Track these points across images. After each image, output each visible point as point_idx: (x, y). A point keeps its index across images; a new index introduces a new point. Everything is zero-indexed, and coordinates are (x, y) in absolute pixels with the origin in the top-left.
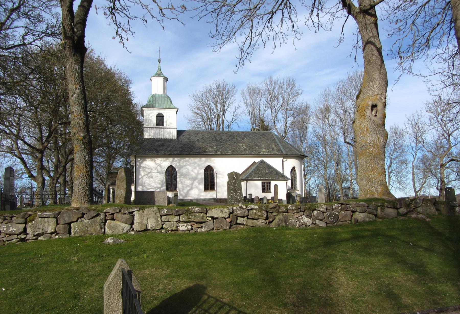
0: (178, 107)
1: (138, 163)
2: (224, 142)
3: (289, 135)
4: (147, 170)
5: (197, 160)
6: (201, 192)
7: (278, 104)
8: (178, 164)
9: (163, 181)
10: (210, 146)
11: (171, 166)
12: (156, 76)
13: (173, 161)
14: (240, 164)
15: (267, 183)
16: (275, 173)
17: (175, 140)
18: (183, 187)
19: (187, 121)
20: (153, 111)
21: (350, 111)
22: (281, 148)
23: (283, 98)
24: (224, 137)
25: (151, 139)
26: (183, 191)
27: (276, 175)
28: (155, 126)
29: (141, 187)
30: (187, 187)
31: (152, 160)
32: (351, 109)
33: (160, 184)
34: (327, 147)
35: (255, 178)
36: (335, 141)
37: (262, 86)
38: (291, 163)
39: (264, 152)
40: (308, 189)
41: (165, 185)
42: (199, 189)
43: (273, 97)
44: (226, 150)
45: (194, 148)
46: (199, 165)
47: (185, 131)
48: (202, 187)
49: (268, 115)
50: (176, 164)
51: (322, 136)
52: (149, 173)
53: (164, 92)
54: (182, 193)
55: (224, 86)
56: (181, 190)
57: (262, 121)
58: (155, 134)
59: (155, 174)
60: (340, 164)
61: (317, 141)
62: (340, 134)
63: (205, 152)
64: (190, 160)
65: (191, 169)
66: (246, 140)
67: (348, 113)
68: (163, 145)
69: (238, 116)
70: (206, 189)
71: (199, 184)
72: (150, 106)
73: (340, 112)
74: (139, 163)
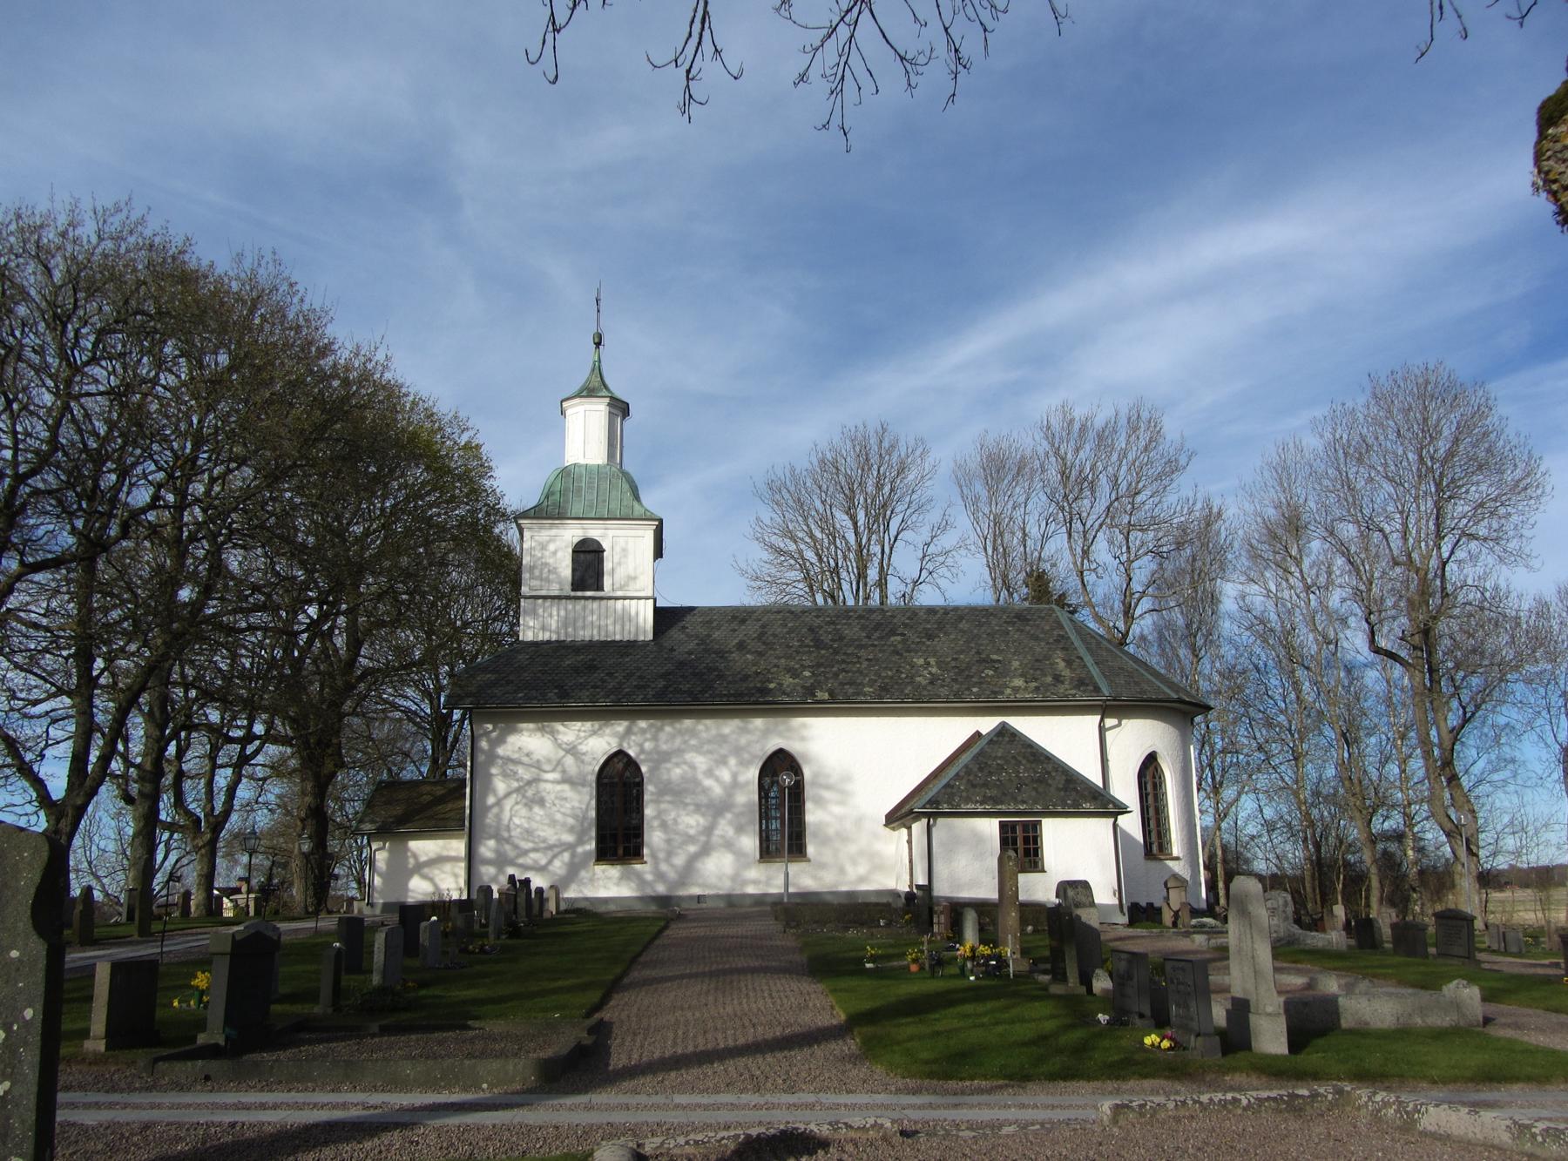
0: (660, 514)
1: (484, 744)
2: (855, 653)
3: (1144, 624)
4: (521, 771)
6: (747, 866)
7: (1094, 508)
10: (789, 670)
11: (620, 753)
12: (578, 395)
13: (628, 732)
15: (1025, 825)
16: (1060, 780)
17: (645, 644)
18: (668, 841)
19: (744, 581)
21: (1387, 529)
22: (1095, 671)
23: (1115, 484)
24: (852, 631)
25: (549, 642)
27: (1065, 789)
28: (568, 591)
29: (492, 843)
30: (685, 843)
31: (542, 730)
33: (571, 830)
34: (1300, 673)
35: (970, 807)
36: (1332, 647)
37: (1029, 442)
38: (1136, 738)
39: (1016, 690)
40: (1232, 840)
41: (593, 834)
42: (739, 854)
43: (1072, 488)
44: (851, 683)
45: (720, 677)
46: (737, 751)
48: (750, 843)
49: (1058, 553)
50: (641, 745)
51: (1278, 628)
52: (529, 783)
54: (664, 867)
55: (886, 444)
56: (661, 855)
57: (1039, 583)
58: (565, 623)
59: (551, 787)
60: (1357, 740)
62: (1352, 621)
63: (764, 691)
65: (704, 767)
66: (943, 644)
68: (591, 668)
69: (942, 565)
70: (767, 852)
71: (740, 829)
72: (549, 510)
73: (1349, 531)
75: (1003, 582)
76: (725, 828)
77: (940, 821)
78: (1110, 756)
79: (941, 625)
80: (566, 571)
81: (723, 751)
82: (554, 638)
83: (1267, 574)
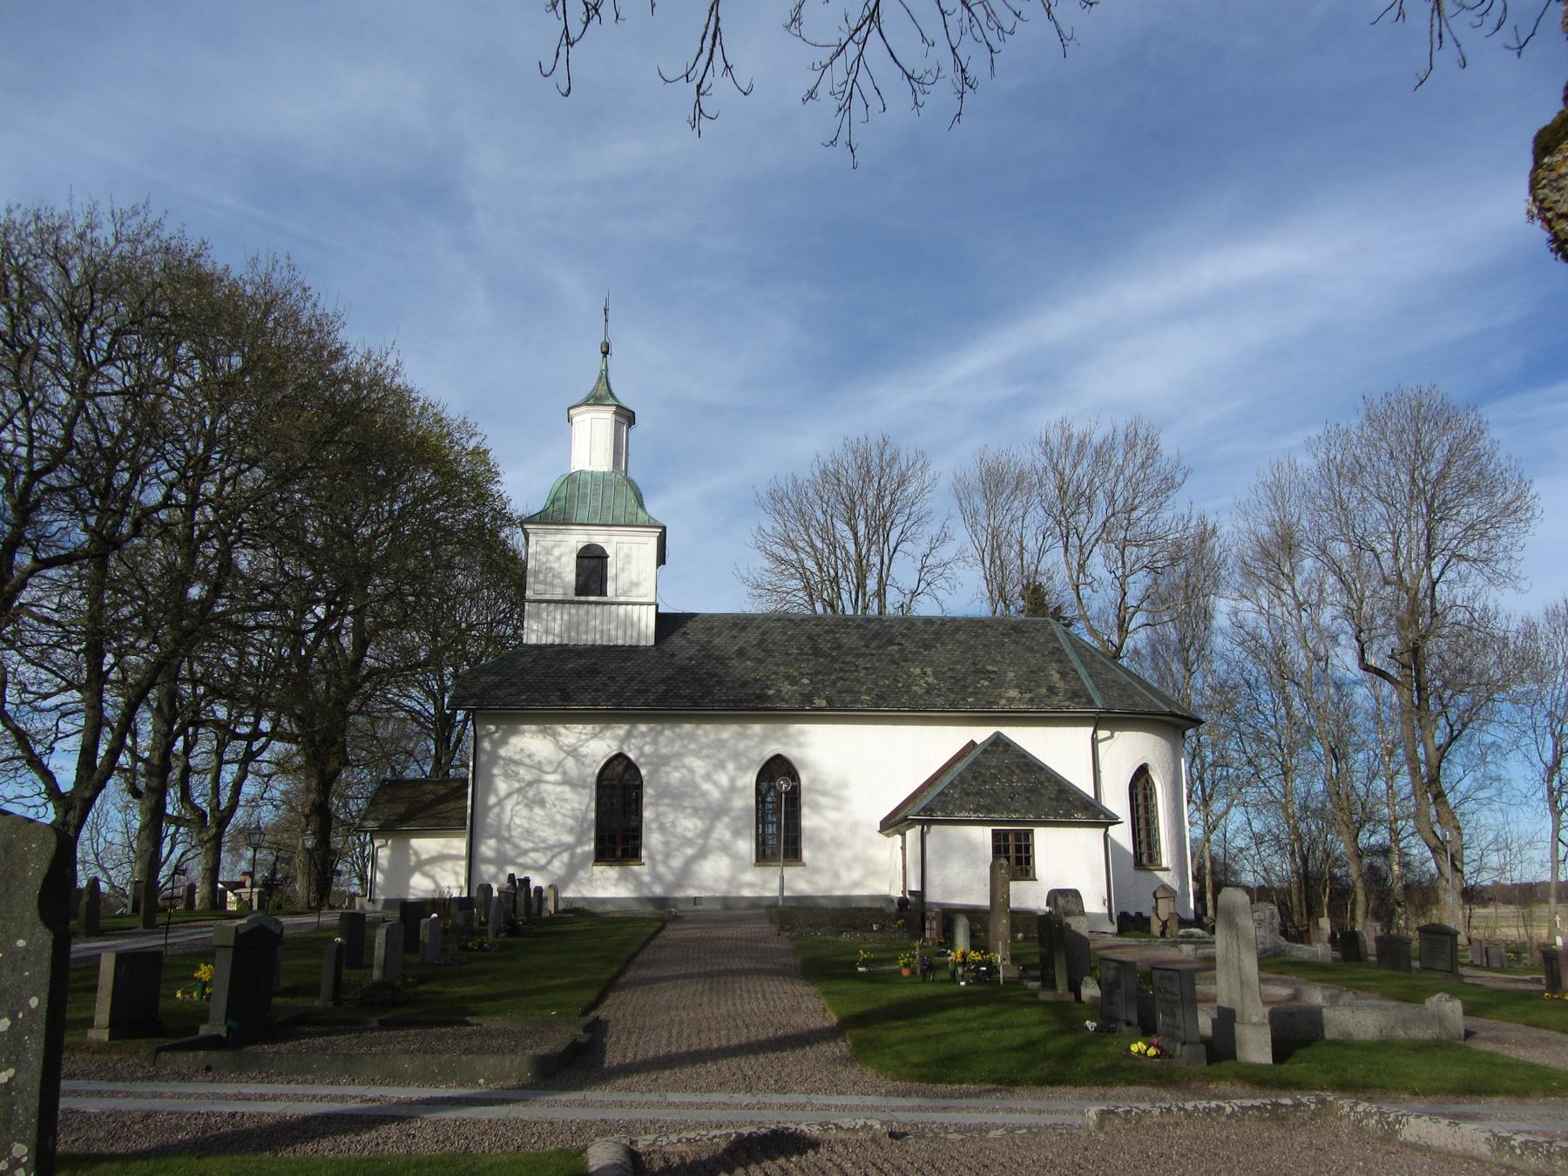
0: (663, 522)
1: (486, 745)
2: (850, 661)
4: (522, 771)
5: (728, 732)
6: (743, 870)
7: (1090, 523)
8: (647, 749)
9: (584, 819)
10: (788, 677)
11: (620, 757)
12: (585, 403)
13: (629, 735)
14: (919, 751)
15: (1017, 834)
16: (1052, 791)
17: (647, 649)
18: (666, 844)
19: (745, 589)
20: (566, 537)
22: (1089, 684)
23: (1112, 500)
24: (850, 640)
25: (552, 645)
26: (665, 862)
28: (571, 595)
29: (492, 842)
31: (544, 732)
32: (1380, 538)
33: (571, 830)
34: (1290, 689)
35: (963, 815)
36: (1322, 664)
37: (1028, 456)
38: (1129, 749)
39: (1011, 700)
40: (1221, 852)
41: (593, 835)
42: (735, 857)
43: (1069, 504)
44: (849, 691)
46: (736, 756)
47: (693, 615)
48: (746, 846)
49: (1055, 567)
50: (641, 749)
51: (1270, 644)
52: (530, 784)
53: (616, 463)
54: (661, 869)
55: (887, 457)
56: (659, 857)
57: (1036, 596)
58: (569, 627)
59: (552, 788)
60: (1345, 756)
61: (1250, 666)
62: (1342, 639)
63: (763, 697)
64: (700, 732)
65: (700, 770)
66: (940, 654)
67: (1368, 555)
68: (593, 671)
69: (943, 579)
70: (763, 856)
71: (737, 833)
72: (554, 516)
73: (1341, 550)
74: (492, 742)
75: (1000, 594)
76: (722, 831)
77: (934, 828)
78: (1103, 768)
79: (938, 636)
80: (570, 576)
81: (722, 756)
82: (557, 641)
83: (1260, 591)
